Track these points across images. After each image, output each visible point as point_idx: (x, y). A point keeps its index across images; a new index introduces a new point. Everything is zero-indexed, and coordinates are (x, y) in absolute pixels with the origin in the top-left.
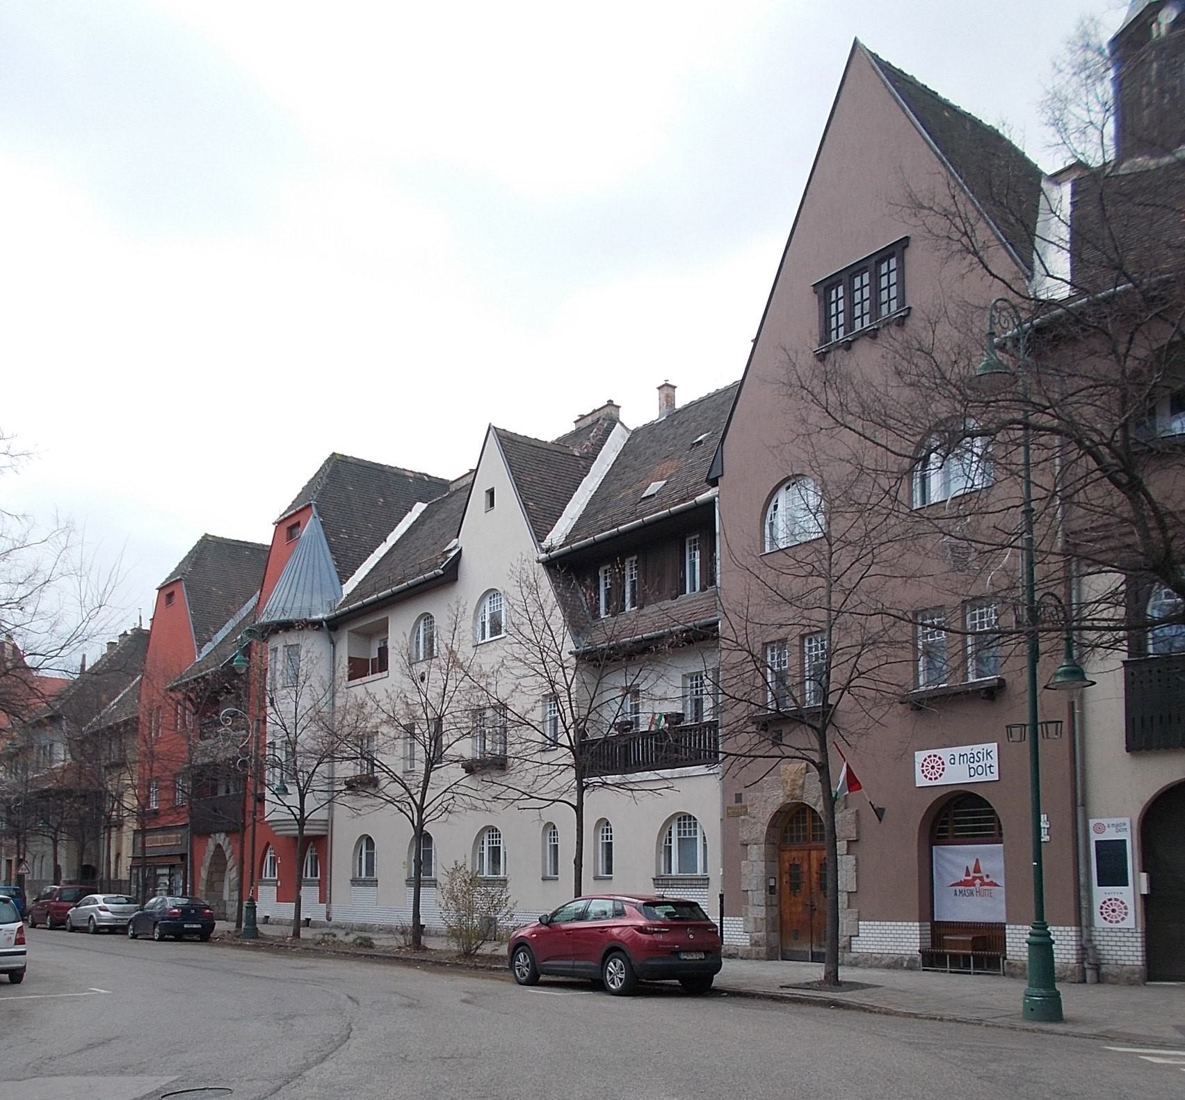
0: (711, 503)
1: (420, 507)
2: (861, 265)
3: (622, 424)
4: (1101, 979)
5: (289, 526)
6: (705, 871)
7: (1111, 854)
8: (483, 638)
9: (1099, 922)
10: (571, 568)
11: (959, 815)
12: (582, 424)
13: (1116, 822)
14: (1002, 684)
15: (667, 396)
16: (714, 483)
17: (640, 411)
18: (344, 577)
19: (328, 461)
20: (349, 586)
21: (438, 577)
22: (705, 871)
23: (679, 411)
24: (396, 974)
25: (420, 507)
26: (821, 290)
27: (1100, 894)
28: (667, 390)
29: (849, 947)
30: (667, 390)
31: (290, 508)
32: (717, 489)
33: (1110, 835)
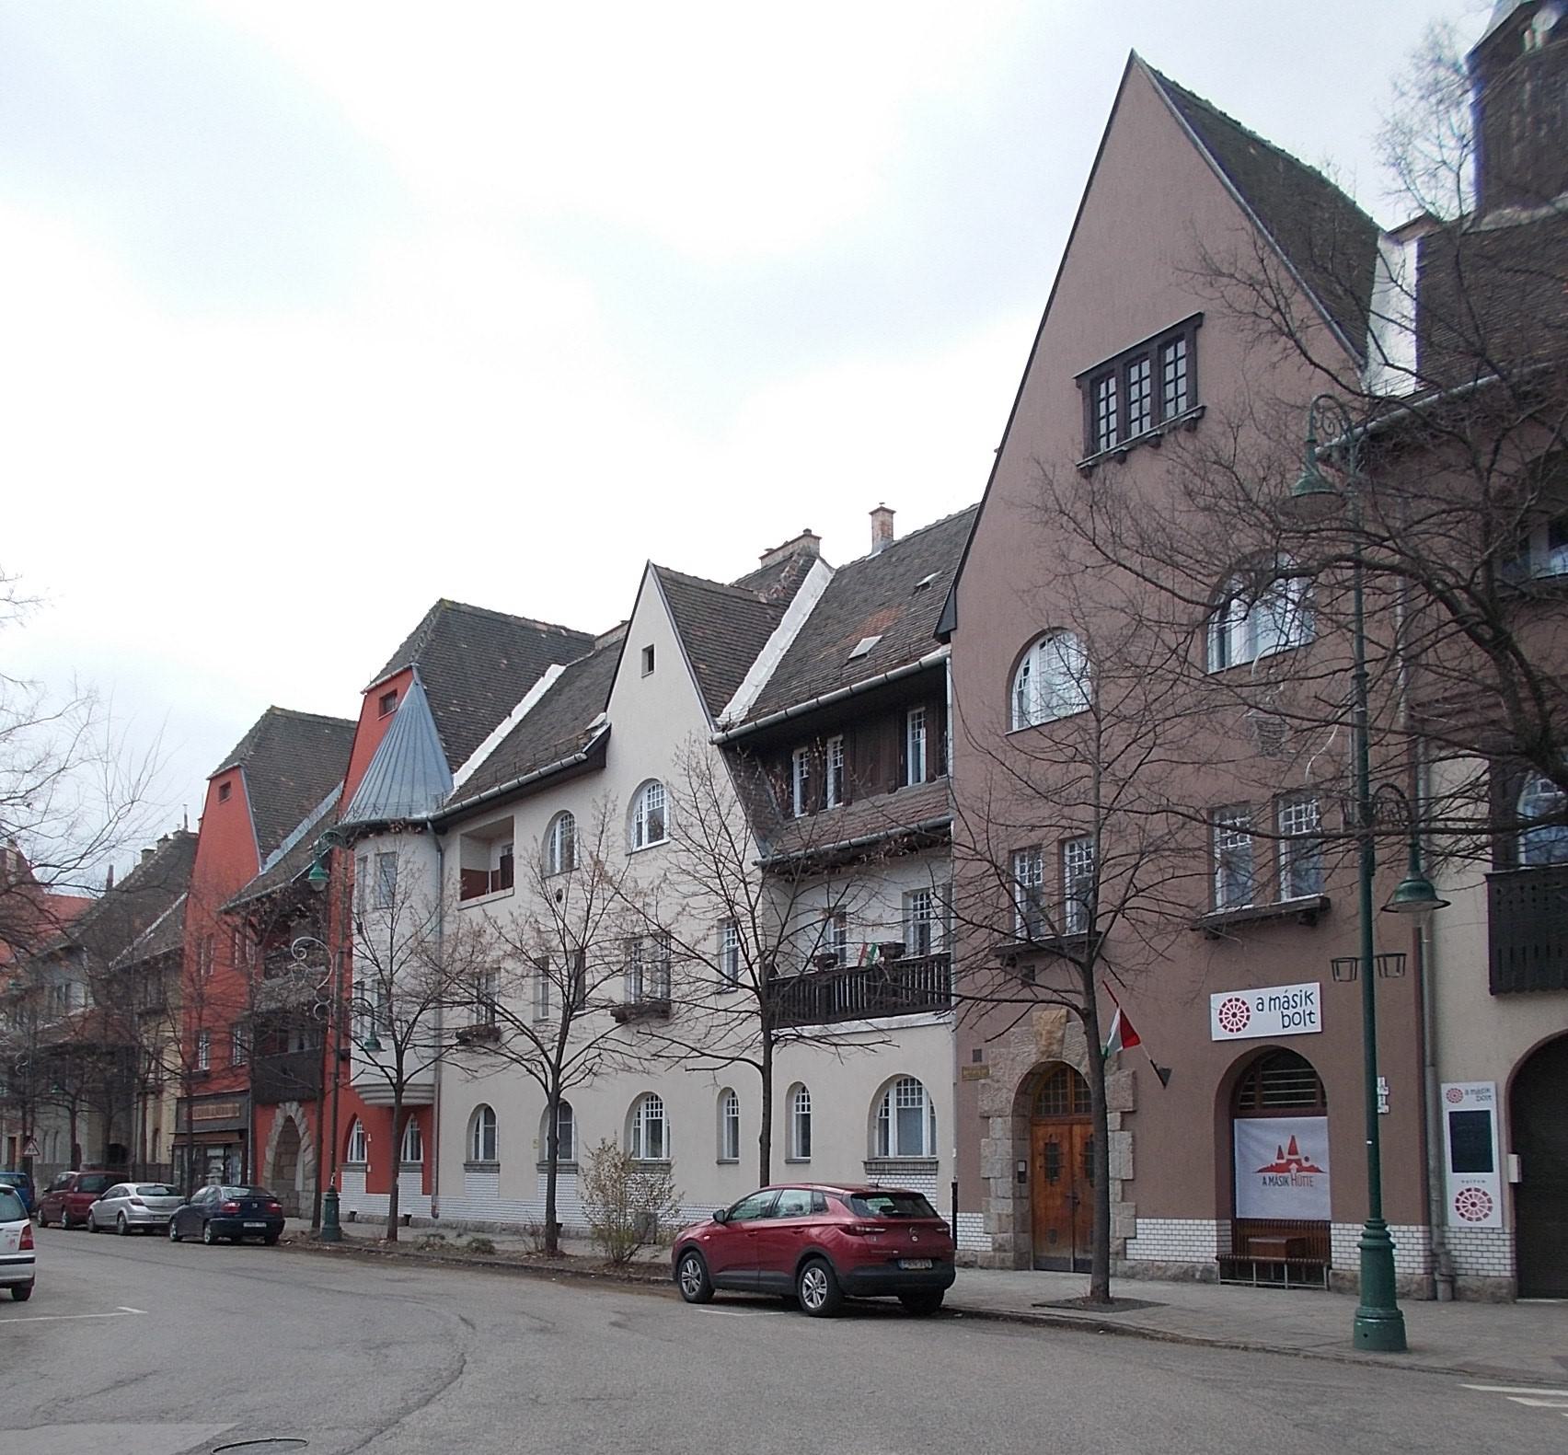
0: (940, 666)
1: (555, 671)
2: (1140, 351)
3: (823, 561)
4: (1456, 1295)
5: (382, 695)
6: (933, 1151)
7: (1470, 1129)
8: (640, 843)
9: (1454, 1219)
10: (756, 752)
11: (1269, 1078)
12: (770, 561)
13: (1476, 1087)
14: (1325, 905)
15: (883, 524)
16: (944, 638)
17: (847, 544)
18: (455, 763)
19: (434, 610)
20: (462, 775)
21: (579, 763)
22: (933, 1151)
23: (899, 543)
24: (524, 1288)
25: (555, 671)
26: (1087, 383)
27: (1456, 1182)
28: (883, 516)
29: (1123, 1252)
30: (883, 516)
31: (383, 672)
32: (948, 647)
33: (1469, 1105)
